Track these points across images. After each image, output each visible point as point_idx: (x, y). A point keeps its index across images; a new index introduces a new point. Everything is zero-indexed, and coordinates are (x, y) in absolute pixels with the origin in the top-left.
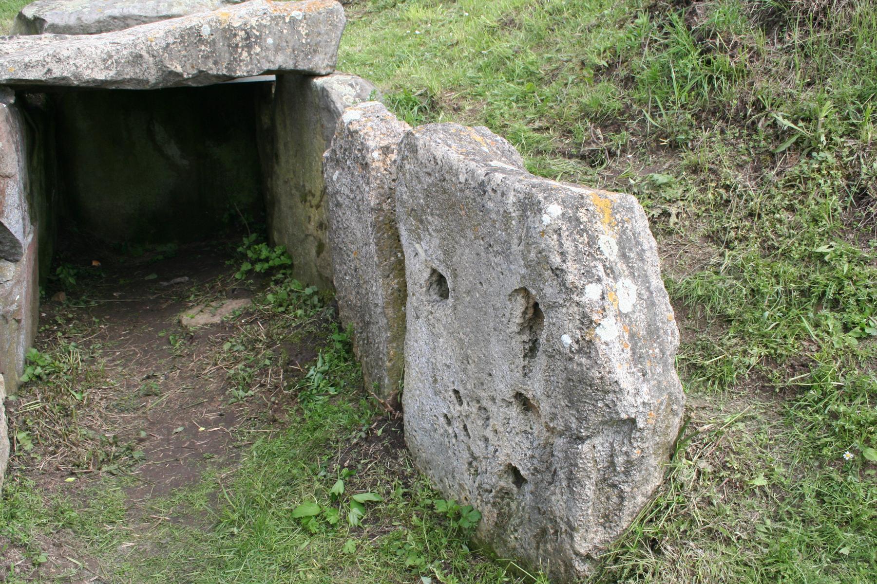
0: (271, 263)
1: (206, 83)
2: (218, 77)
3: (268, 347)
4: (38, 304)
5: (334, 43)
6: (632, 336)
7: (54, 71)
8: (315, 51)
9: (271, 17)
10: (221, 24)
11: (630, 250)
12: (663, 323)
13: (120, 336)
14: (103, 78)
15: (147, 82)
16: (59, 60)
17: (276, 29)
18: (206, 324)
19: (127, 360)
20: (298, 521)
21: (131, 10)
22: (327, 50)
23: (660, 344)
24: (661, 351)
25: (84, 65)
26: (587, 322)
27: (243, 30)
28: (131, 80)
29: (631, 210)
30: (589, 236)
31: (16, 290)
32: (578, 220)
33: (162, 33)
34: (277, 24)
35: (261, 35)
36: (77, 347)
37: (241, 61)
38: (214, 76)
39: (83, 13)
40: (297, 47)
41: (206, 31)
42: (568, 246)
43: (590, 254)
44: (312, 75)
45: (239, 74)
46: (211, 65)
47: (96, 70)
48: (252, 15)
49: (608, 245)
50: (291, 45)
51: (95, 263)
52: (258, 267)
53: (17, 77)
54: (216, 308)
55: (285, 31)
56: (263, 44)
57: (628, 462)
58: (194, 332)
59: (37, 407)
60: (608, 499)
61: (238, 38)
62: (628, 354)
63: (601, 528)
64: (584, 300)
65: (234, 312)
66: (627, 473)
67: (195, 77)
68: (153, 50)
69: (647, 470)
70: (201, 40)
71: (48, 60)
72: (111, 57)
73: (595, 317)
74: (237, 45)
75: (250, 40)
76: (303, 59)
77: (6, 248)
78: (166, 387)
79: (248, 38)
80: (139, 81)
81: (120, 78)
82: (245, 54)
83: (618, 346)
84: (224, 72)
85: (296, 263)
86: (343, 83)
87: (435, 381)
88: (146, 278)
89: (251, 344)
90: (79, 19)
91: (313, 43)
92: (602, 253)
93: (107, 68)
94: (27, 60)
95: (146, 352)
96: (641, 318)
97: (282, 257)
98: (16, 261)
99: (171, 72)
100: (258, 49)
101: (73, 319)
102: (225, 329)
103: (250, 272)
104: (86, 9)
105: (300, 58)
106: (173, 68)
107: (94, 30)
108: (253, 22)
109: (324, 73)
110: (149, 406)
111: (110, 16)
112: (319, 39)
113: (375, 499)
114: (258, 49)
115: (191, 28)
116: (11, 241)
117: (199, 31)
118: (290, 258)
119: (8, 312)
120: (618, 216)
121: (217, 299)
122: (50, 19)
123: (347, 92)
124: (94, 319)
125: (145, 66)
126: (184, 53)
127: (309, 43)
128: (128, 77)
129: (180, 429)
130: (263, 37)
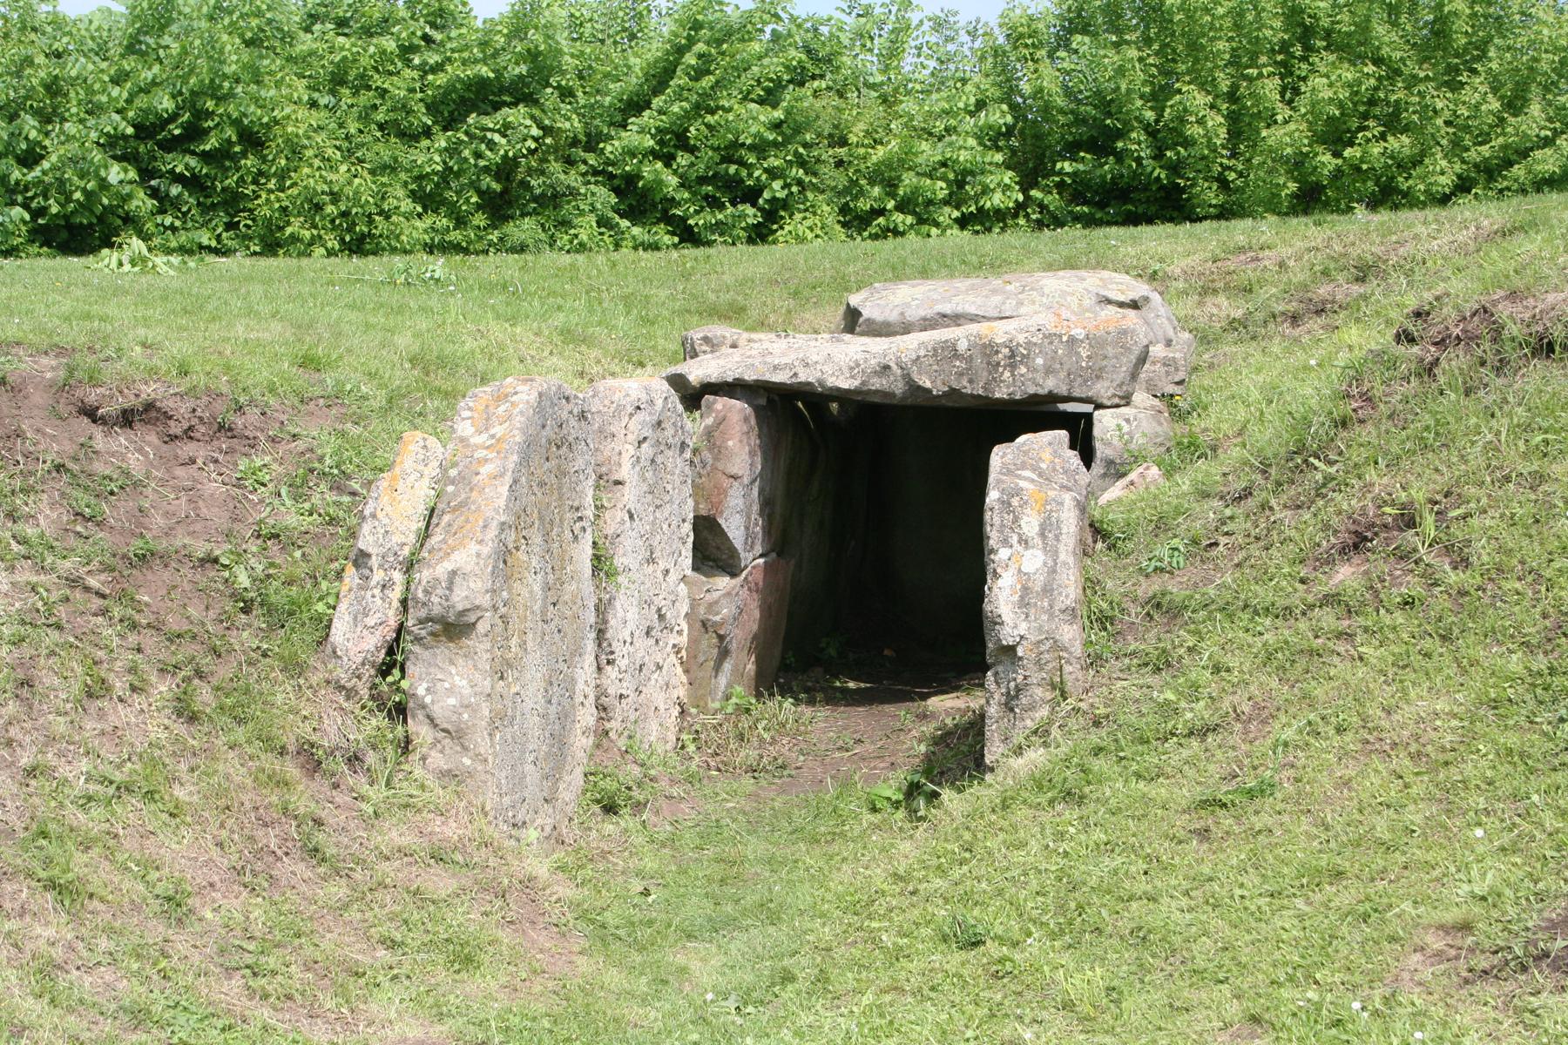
2: (972, 396)
6: (1025, 589)
8: (1098, 377)
15: (893, 395)
28: (876, 392)
29: (1062, 504)
32: (1010, 505)
33: (915, 345)
41: (962, 346)
45: (997, 395)
46: (965, 383)
49: (1030, 524)
50: (1066, 367)
62: (1016, 598)
66: (1017, 697)
70: (956, 355)
72: (858, 365)
74: (998, 364)
79: (1013, 356)
83: (1008, 591)
93: (852, 377)
99: (919, 387)
100: (1023, 370)
108: (1021, 339)
114: (1023, 370)
117: (954, 345)
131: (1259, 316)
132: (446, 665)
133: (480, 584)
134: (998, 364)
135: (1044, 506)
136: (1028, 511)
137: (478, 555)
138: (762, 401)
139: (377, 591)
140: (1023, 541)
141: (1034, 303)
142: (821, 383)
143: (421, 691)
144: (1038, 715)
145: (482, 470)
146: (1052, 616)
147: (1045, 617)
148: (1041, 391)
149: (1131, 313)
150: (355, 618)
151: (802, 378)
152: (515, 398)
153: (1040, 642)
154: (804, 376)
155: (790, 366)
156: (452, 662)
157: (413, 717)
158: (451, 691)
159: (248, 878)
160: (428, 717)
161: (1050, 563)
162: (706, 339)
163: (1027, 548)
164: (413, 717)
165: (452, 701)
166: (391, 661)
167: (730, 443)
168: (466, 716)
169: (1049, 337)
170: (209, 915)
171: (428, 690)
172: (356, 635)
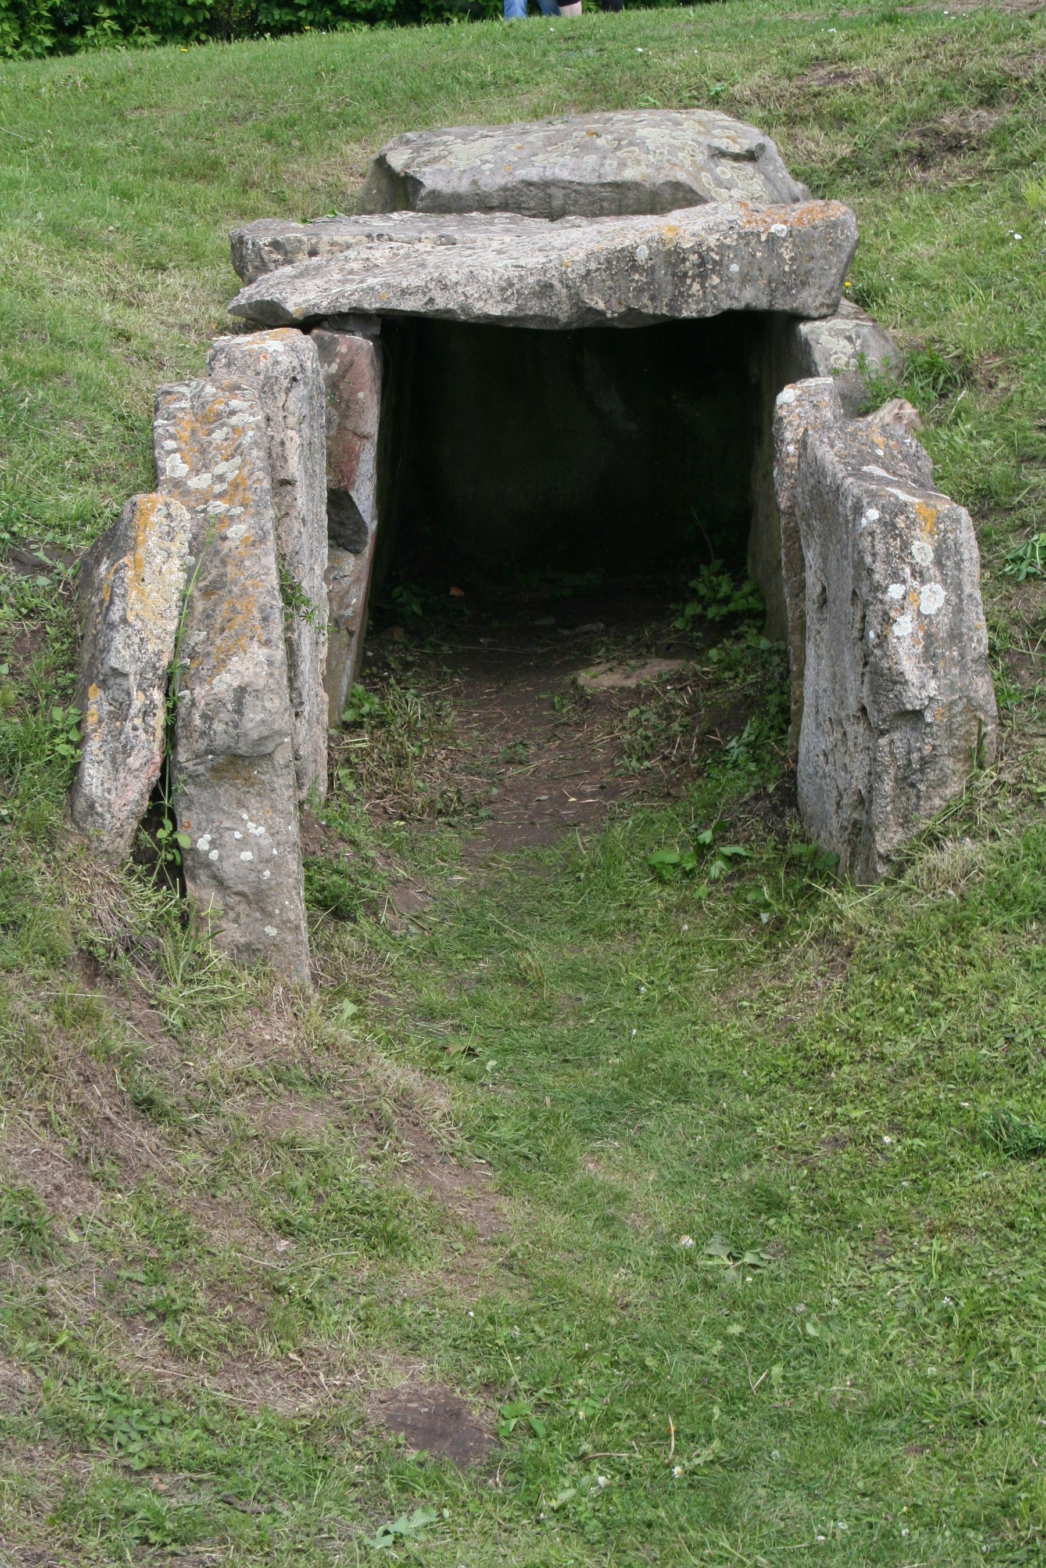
0: (732, 606)
1: (640, 324)
2: (654, 316)
3: (688, 714)
4: (364, 635)
5: (834, 271)
6: (929, 636)
7: (438, 300)
8: (804, 284)
9: (739, 234)
10: (664, 245)
11: (948, 558)
12: (970, 629)
13: (483, 694)
14: (498, 313)
15: (557, 320)
16: (445, 287)
17: (744, 252)
18: (613, 688)
19: (487, 724)
20: (653, 868)
21: (557, 171)
22: (823, 281)
23: (960, 648)
24: (960, 654)
25: (476, 295)
26: (887, 620)
27: (695, 252)
28: (535, 316)
29: (958, 521)
30: (902, 541)
31: (353, 590)
32: (894, 526)
33: (582, 255)
34: (747, 244)
35: (721, 260)
36: (417, 697)
37: (689, 296)
38: (648, 316)
39: (482, 172)
40: (775, 276)
41: (642, 254)
42: (880, 548)
43: (900, 557)
44: (797, 317)
45: (685, 314)
46: (646, 301)
47: (490, 302)
48: (710, 230)
49: (923, 550)
50: (766, 274)
51: (454, 591)
52: (711, 613)
53: (390, 306)
54: (634, 668)
55: (759, 254)
56: (724, 272)
57: (922, 758)
58: (592, 696)
59: (364, 745)
60: (908, 799)
61: (688, 264)
62: (919, 649)
63: (900, 829)
64: (887, 598)
65: (660, 676)
66: (922, 771)
67: (622, 317)
68: (568, 279)
69: (941, 770)
70: (635, 267)
71: (431, 286)
72: (511, 285)
73: (892, 614)
74: (685, 274)
75: (705, 266)
76: (784, 295)
77: (348, 532)
78: (537, 756)
79: (703, 263)
80: (545, 319)
81: (521, 314)
82: (696, 287)
84: (664, 312)
85: (768, 608)
86: (837, 333)
87: (817, 712)
88: (536, 623)
89: (667, 713)
90: (475, 182)
91: (802, 271)
92: (913, 557)
93: (505, 300)
94: (404, 284)
95: (517, 717)
96: (944, 624)
97: (750, 599)
98: (357, 553)
99: (590, 309)
100: (716, 280)
101: (413, 664)
102: (637, 696)
103: (699, 621)
104: (488, 166)
105: (778, 294)
106: (592, 304)
107: (495, 203)
108: (712, 241)
109: (815, 314)
110: (509, 774)
111: (523, 181)
112: (811, 265)
113: (744, 853)
114: (716, 280)
115: (623, 250)
116: (356, 524)
117: (632, 254)
118: (762, 600)
119: (342, 616)
120: (942, 526)
121: (640, 656)
122: (431, 180)
123: (839, 348)
124: (445, 669)
125: (555, 299)
126: (609, 283)
127: (794, 272)
128: (532, 313)
129: (544, 798)
130: (725, 262)
131: (873, 156)
132: (233, 809)
133: (277, 702)
134: (685, 275)
135: (936, 524)
136: (917, 532)
137: (270, 663)
138: (376, 330)
139: (138, 722)
140: (919, 574)
141: (638, 162)
142: (464, 308)
143: (203, 844)
144: (948, 792)
145: (231, 532)
146: (964, 669)
147: (956, 671)
148: (736, 305)
149: (749, 167)
150: (113, 761)
151: (440, 303)
152: (234, 420)
153: (953, 703)
154: (442, 302)
155: (424, 290)
156: (241, 804)
157: (194, 878)
158: (244, 843)
159: (94, 1167)
160: (215, 877)
161: (954, 599)
162: (276, 245)
163: (923, 583)
164: (194, 878)
165: (247, 856)
166: (159, 808)
167: (361, 395)
168: (267, 873)
169: (743, 236)
170: (73, 1237)
171: (212, 843)
172: (115, 787)
